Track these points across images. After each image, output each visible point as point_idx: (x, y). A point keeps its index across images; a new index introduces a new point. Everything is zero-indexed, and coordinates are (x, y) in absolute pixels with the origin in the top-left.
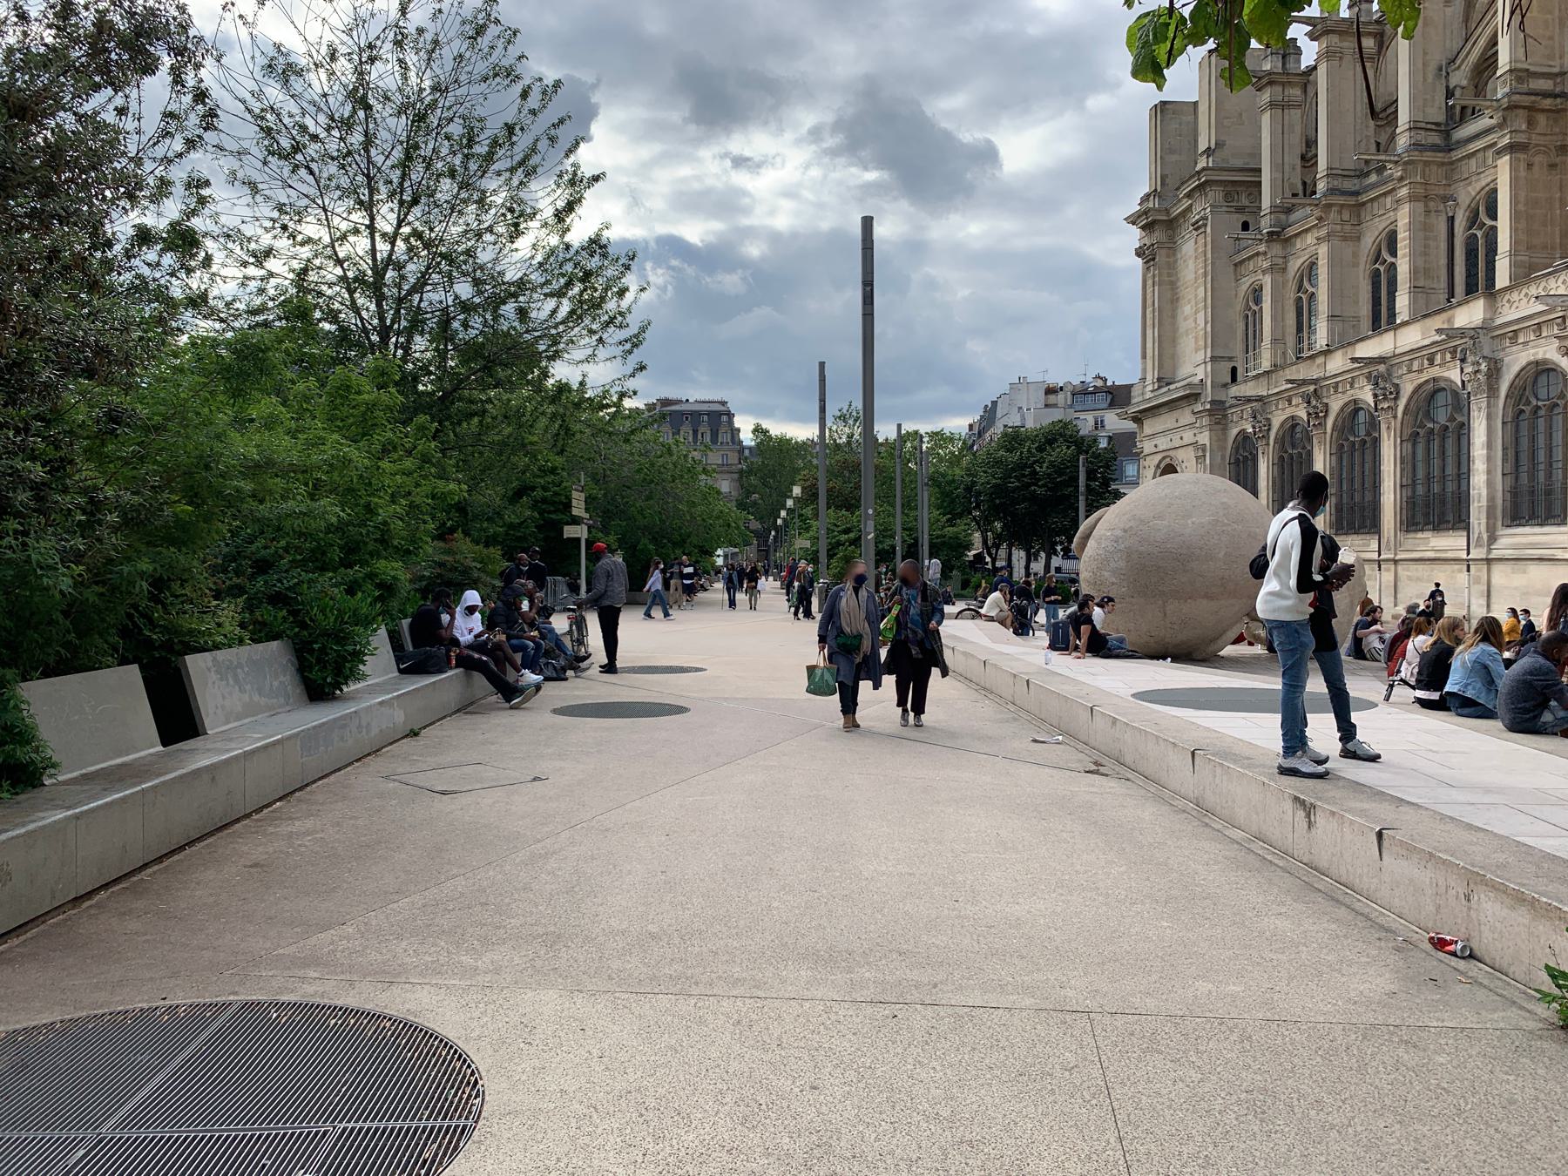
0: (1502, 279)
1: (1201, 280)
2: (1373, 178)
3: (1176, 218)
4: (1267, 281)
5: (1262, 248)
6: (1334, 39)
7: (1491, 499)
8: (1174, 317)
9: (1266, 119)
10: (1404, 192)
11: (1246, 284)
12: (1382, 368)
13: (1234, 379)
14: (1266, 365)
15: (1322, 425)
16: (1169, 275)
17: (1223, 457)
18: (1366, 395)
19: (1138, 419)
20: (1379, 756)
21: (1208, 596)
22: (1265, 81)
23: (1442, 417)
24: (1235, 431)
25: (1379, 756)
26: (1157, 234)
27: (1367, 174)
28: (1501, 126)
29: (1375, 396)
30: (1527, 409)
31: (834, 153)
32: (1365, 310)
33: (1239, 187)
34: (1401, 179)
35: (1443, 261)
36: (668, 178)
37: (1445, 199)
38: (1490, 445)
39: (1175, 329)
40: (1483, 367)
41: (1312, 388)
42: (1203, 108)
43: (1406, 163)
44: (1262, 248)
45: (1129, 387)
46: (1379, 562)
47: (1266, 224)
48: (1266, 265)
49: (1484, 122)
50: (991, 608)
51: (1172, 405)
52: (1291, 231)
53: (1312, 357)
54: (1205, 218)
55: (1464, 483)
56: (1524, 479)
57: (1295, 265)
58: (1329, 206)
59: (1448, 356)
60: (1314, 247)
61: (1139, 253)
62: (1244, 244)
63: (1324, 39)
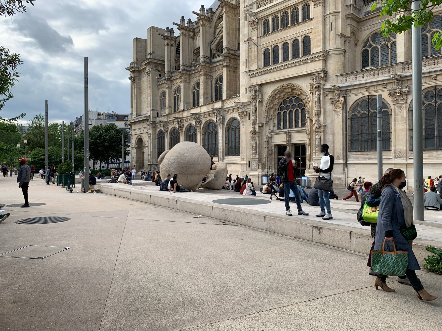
0: (224, 97)
1: (149, 88)
2: (193, 68)
4: (167, 91)
5: (166, 82)
6: (184, 31)
7: (223, 149)
8: (140, 97)
9: (166, 47)
10: (201, 73)
11: (161, 91)
12: (197, 116)
14: (167, 113)
15: (182, 129)
16: (139, 86)
17: (155, 137)
18: (194, 123)
19: (130, 125)
20: (308, 214)
21: (198, 174)
22: (166, 38)
23: (212, 129)
24: (158, 130)
25: (308, 214)
26: (135, 74)
27: (192, 67)
28: (224, 60)
29: (196, 123)
31: (14, 30)
32: (192, 101)
33: (159, 65)
34: (201, 69)
35: (210, 91)
37: (211, 76)
38: (223, 137)
39: (141, 101)
40: (221, 118)
41: (180, 120)
42: (149, 42)
43: (202, 66)
44: (166, 82)
45: (127, 116)
47: (166, 76)
48: (166, 86)
49: (220, 58)
50: (121, 179)
51: (141, 122)
52: (173, 78)
53: (179, 112)
55: (217, 145)
56: (230, 145)
57: (174, 87)
58: (183, 73)
59: (213, 115)
60: (179, 83)
61: (130, 78)
62: (160, 80)
63: (181, 30)
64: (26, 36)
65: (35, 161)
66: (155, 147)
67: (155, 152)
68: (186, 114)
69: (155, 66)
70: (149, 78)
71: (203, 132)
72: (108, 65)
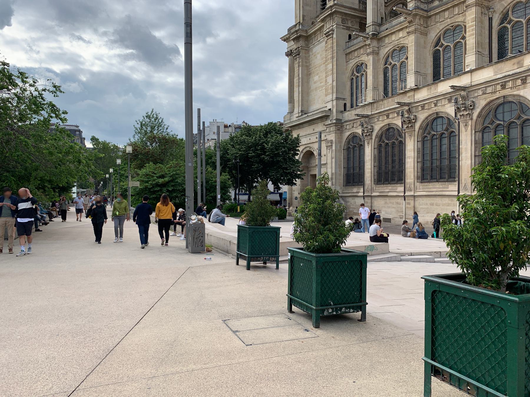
1: (330, 61)
3: (310, 36)
4: (369, 60)
5: (368, 42)
8: (308, 82)
11: (352, 63)
13: (345, 110)
14: (369, 100)
16: (306, 63)
17: (340, 146)
18: (398, 122)
24: (347, 134)
26: (301, 42)
30: (429, 137)
31: (114, 42)
32: (430, 70)
36: (46, 47)
39: (309, 88)
41: (407, 108)
46: (404, 197)
54: (333, 30)
58: (416, 15)
64: (127, 47)
65: (146, 187)
66: (340, 165)
67: (340, 175)
68: (423, 94)
69: (343, 21)
70: (330, 41)
71: (479, 127)
72: (217, 80)
